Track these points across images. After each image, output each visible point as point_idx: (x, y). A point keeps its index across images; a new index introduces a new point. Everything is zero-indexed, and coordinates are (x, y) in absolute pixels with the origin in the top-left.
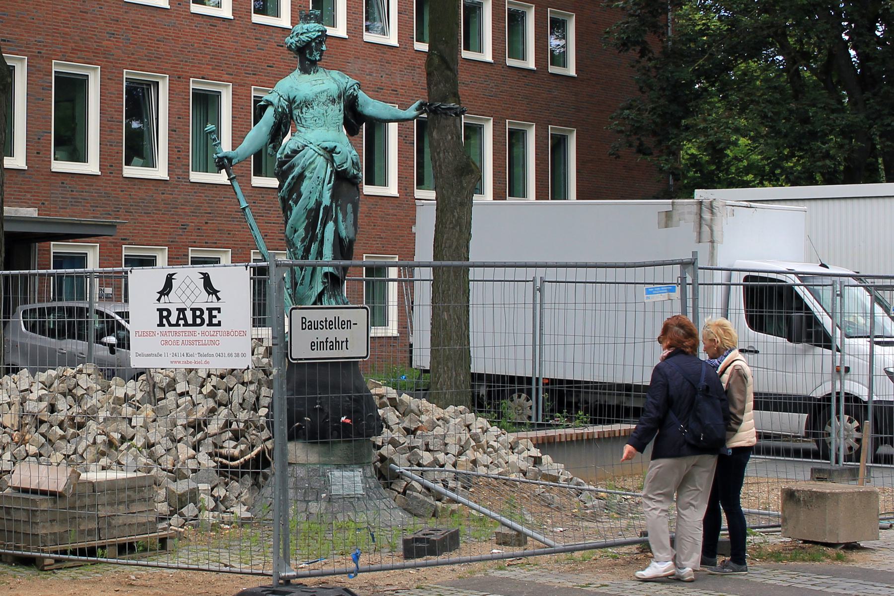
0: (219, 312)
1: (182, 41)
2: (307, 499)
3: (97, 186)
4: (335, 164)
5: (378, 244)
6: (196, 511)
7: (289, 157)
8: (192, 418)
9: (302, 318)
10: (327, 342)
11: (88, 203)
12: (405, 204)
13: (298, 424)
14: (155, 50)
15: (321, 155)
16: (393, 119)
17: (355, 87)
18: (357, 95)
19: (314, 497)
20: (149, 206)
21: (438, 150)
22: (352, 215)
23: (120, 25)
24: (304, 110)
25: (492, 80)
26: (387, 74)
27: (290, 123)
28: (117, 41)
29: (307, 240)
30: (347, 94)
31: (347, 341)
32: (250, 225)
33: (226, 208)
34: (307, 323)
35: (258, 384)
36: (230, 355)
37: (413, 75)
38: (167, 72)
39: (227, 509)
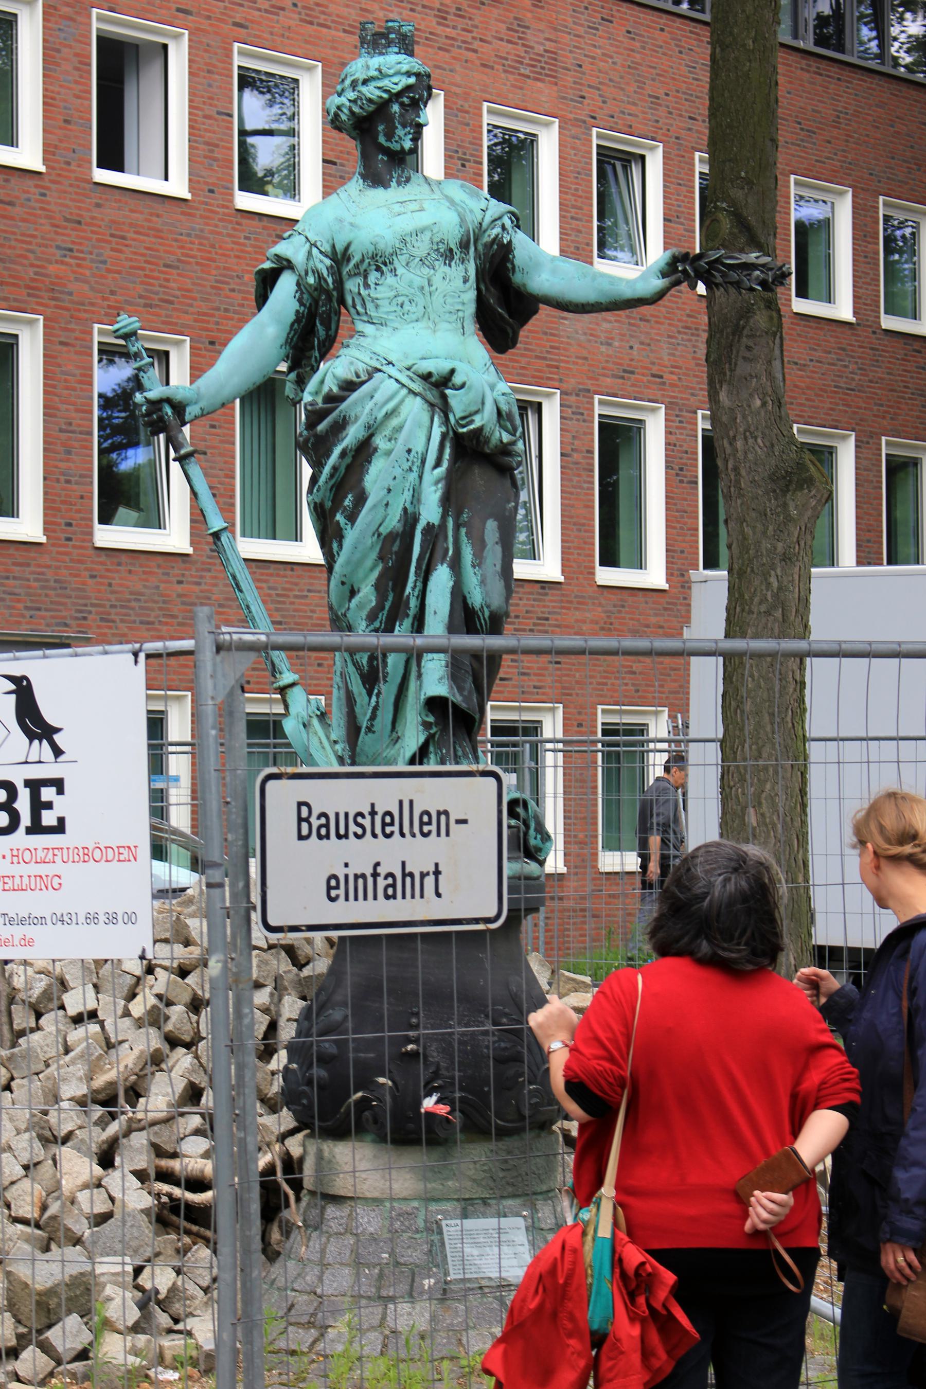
0: (60, 791)
1: (218, 268)
2: (384, 1293)
3: (39, 566)
4: (451, 417)
5: (626, 684)
6: (86, 1337)
7: (333, 400)
8: (100, 1081)
9: (300, 804)
10: (375, 875)
11: (19, 601)
12: (681, 604)
13: (360, 1094)
14: (161, 286)
15: (416, 394)
16: (603, 300)
17: (507, 221)
18: (510, 242)
19: (403, 1287)
20: (152, 609)
21: (731, 433)
22: (499, 549)
23: (84, 231)
24: (373, 277)
25: (853, 357)
26: (642, 343)
27: (339, 314)
28: (78, 265)
29: (383, 615)
30: (486, 239)
31: (437, 873)
32: (234, 577)
33: (313, 611)
34: (313, 820)
35: (275, 988)
36: (92, 919)
37: (694, 346)
38: (186, 331)
39: (176, 1321)
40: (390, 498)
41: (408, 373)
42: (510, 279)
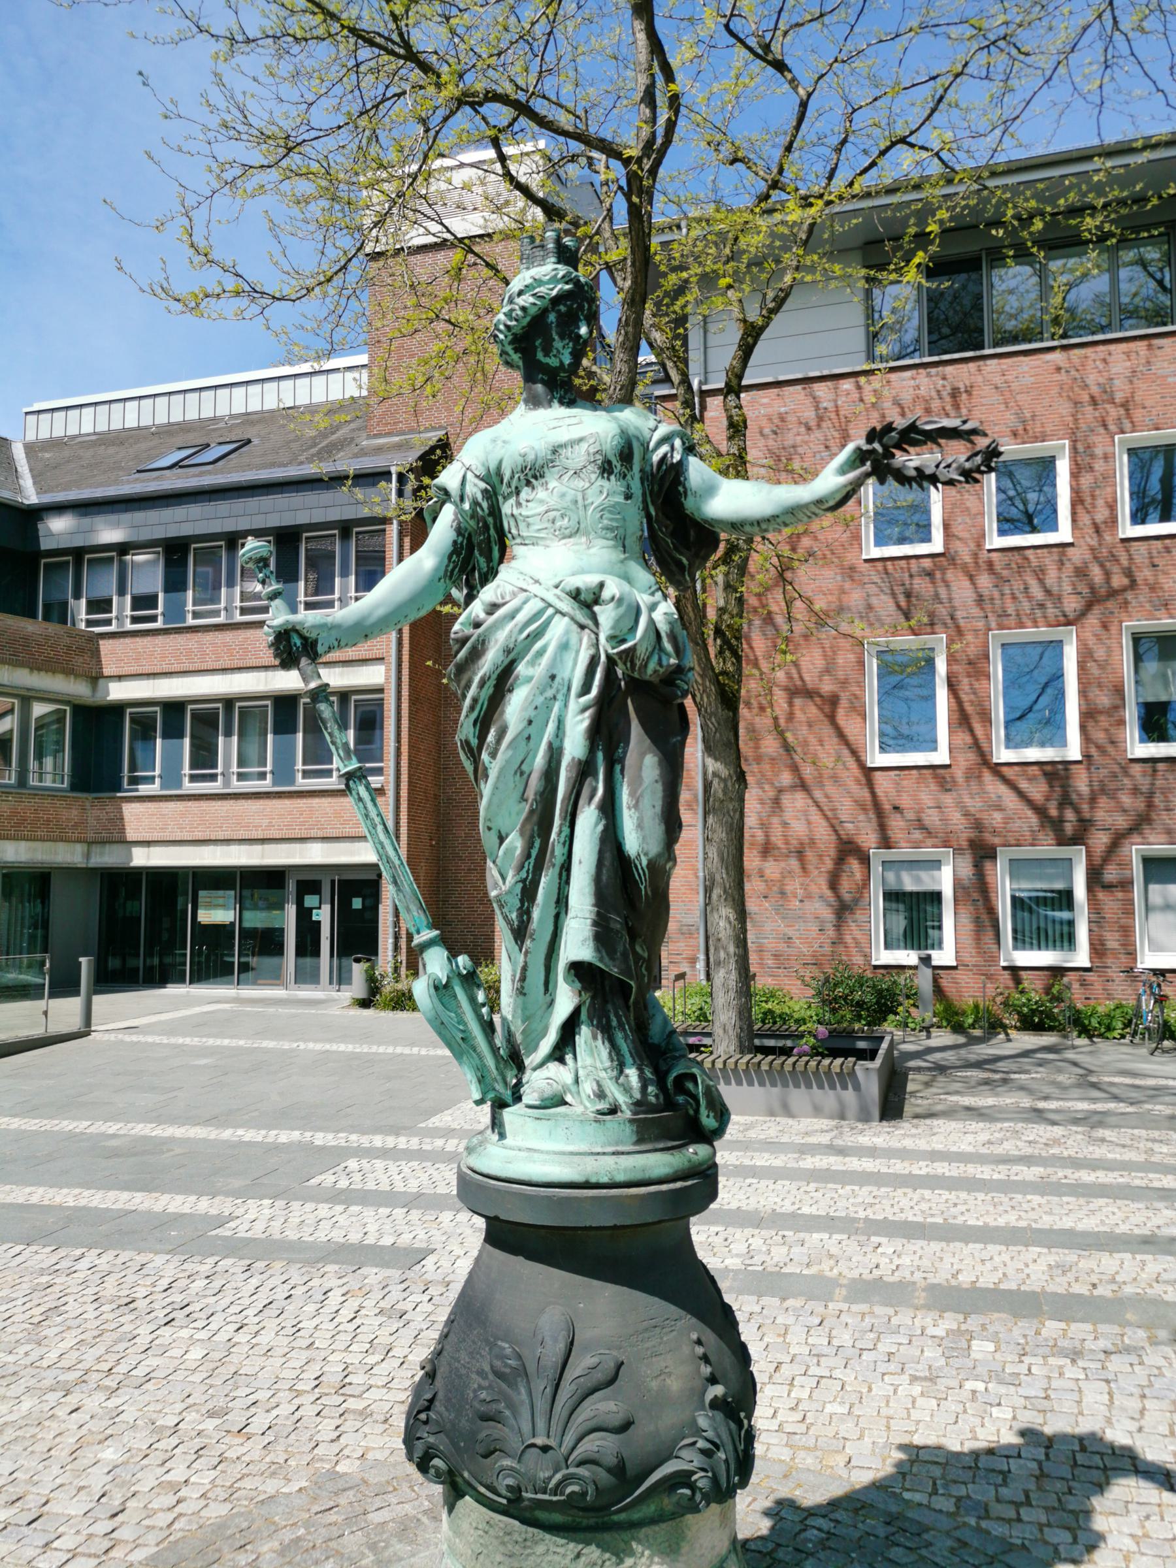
15: (564, 615)
40: (532, 730)
41: (558, 591)
42: (682, 505)
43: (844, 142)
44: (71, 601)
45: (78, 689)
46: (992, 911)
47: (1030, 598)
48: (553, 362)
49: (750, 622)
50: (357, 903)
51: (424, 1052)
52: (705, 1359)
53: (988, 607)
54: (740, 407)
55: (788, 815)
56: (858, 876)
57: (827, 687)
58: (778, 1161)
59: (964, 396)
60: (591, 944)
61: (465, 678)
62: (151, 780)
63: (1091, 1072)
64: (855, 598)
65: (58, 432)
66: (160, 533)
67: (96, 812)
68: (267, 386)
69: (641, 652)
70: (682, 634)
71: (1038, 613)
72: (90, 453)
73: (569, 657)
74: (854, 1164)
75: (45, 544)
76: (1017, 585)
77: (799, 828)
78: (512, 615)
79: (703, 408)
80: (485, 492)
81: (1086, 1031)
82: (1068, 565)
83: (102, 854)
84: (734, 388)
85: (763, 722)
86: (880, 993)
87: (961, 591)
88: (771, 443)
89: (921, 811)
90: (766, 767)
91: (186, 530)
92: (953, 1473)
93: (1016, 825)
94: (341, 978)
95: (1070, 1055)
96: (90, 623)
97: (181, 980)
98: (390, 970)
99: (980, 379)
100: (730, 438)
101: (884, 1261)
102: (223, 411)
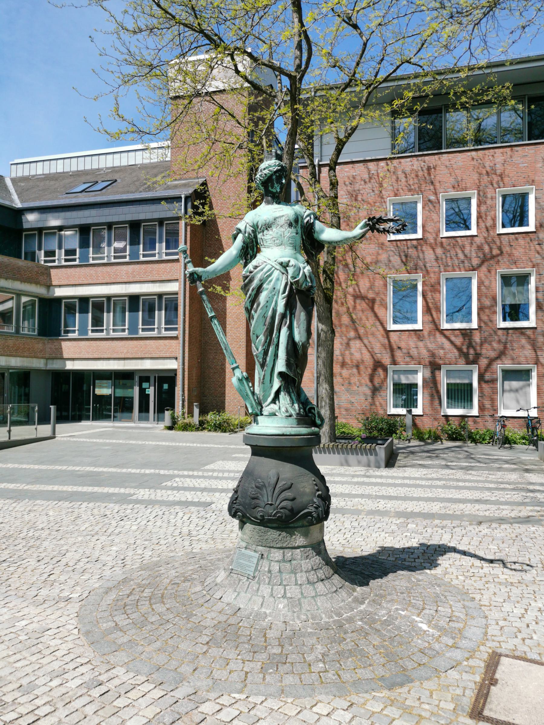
40: (268, 304)
43: (382, 60)
44: (37, 251)
45: (41, 291)
46: (438, 392)
47: (458, 259)
48: (274, 191)
49: (338, 267)
50: (166, 386)
51: (199, 445)
52: (316, 485)
53: (440, 262)
54: (335, 176)
55: (353, 350)
56: (382, 377)
57: (371, 295)
58: (345, 479)
59: (433, 170)
60: (285, 366)
61: (247, 288)
62: (74, 331)
63: (472, 454)
64: (383, 257)
65: (26, 173)
66: (78, 222)
67: (50, 346)
68: (123, 154)
69: (301, 281)
70: (313, 276)
71: (461, 265)
72: (42, 184)
73: (279, 283)
74: (373, 480)
75: (25, 226)
76: (453, 253)
77: (357, 356)
78: (262, 270)
79: (320, 172)
80: (253, 231)
81: (474, 441)
82: (475, 245)
83: (53, 364)
84: (332, 167)
85: (343, 309)
86: (390, 425)
87: (429, 255)
88: (349, 188)
89: (409, 349)
90: (344, 329)
91: (90, 221)
92: (395, 552)
93: (449, 356)
94: (159, 419)
95: (465, 449)
96: (46, 261)
97: (88, 418)
98: (180, 413)
99: (439, 162)
100: (331, 189)
101: (380, 506)
102: (102, 166)
